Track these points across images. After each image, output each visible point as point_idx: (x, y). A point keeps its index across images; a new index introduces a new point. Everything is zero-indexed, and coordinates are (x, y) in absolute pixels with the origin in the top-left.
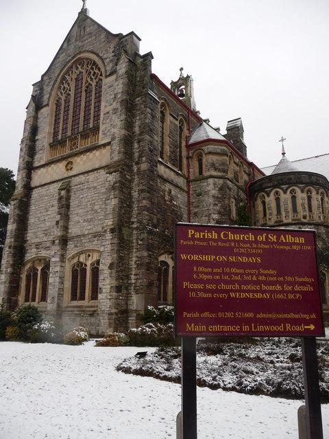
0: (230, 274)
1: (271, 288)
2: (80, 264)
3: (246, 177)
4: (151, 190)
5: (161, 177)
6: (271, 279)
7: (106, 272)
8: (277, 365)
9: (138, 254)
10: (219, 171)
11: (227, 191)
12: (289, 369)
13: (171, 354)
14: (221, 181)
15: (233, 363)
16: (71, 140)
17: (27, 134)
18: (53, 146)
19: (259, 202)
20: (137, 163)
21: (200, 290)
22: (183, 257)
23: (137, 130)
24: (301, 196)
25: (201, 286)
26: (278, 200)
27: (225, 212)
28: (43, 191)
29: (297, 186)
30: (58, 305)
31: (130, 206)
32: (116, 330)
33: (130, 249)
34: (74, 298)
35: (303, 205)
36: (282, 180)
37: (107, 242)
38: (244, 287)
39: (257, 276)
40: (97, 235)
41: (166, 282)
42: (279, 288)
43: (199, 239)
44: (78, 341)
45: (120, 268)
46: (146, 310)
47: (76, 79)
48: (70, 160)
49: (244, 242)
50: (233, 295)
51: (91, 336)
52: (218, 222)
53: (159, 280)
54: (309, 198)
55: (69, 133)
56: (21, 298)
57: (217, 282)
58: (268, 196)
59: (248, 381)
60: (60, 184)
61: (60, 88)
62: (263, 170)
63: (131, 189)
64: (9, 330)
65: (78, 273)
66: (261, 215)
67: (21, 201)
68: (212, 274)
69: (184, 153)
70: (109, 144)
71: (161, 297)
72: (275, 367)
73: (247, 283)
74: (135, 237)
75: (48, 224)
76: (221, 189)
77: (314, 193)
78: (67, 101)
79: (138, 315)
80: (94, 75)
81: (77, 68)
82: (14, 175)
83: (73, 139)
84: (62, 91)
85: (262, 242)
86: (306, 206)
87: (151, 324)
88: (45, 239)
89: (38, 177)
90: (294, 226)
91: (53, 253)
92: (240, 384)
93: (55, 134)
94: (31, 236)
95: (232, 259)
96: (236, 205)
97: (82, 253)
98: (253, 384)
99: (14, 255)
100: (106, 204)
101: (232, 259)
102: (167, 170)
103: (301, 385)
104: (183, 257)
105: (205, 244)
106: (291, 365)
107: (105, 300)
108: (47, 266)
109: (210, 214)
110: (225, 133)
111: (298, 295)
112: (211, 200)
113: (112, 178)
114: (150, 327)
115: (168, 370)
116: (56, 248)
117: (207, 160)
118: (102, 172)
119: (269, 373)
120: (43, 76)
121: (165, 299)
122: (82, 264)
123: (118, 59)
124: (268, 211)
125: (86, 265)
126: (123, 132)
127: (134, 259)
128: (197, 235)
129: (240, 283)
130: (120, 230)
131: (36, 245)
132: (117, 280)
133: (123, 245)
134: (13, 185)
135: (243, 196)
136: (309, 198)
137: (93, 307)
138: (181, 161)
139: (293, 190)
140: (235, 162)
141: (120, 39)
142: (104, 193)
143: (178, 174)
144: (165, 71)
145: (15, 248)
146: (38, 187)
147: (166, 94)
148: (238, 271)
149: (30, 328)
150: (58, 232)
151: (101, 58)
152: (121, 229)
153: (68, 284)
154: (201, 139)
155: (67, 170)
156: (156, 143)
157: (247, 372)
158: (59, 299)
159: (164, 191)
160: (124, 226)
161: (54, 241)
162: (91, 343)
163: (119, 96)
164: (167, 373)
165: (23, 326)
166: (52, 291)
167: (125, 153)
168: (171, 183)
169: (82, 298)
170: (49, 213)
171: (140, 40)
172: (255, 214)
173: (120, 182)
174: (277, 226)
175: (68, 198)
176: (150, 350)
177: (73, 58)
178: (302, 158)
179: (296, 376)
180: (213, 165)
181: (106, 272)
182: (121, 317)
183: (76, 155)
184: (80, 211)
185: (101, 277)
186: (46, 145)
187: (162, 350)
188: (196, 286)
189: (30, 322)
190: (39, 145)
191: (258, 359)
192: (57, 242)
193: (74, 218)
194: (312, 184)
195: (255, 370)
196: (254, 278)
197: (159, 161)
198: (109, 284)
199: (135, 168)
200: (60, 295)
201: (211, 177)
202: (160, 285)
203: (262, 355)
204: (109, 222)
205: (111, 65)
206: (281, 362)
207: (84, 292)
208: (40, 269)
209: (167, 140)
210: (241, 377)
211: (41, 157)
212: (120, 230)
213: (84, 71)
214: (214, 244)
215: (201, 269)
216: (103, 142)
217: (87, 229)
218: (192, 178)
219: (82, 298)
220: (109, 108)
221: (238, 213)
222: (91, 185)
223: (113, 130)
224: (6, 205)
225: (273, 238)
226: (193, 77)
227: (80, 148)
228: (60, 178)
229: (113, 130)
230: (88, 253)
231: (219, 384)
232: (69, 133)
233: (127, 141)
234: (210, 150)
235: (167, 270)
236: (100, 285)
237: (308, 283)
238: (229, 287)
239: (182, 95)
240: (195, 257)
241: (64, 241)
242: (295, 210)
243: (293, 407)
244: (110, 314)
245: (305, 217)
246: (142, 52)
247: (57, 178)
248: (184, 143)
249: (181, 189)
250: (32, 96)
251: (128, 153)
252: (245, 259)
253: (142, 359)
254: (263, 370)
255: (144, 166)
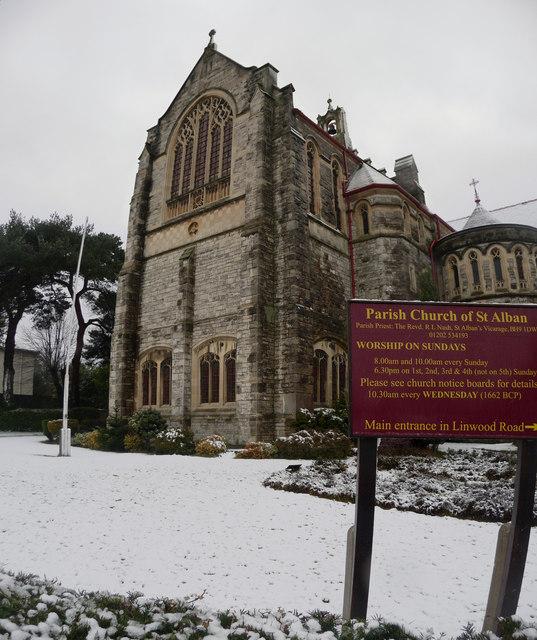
0: (423, 367)
1: (480, 385)
2: (210, 355)
3: (428, 235)
4: (301, 256)
5: (313, 238)
6: (480, 372)
7: (244, 365)
8: (470, 483)
9: (286, 342)
10: (392, 227)
11: (404, 253)
12: (485, 487)
13: (332, 467)
14: (395, 241)
15: (412, 480)
16: (194, 195)
17: (138, 190)
18: (170, 204)
19: (448, 266)
20: (281, 222)
21: (383, 389)
22: (360, 345)
23: (278, 178)
24: (507, 258)
25: (384, 384)
26: (474, 264)
27: (402, 282)
28: (160, 261)
29: (477, 248)
30: (186, 408)
31: (274, 279)
32: (260, 439)
33: (275, 335)
34: (204, 399)
35: (510, 269)
36: (479, 236)
37: (245, 327)
38: (442, 384)
39: (461, 369)
40: (231, 318)
41: (324, 378)
42: (489, 384)
43: (381, 321)
44: (214, 453)
45: (263, 359)
46: (298, 412)
47: (201, 121)
48: (193, 220)
49: (442, 323)
50: (426, 394)
51: (230, 446)
52: (392, 297)
53: (315, 374)
54: (519, 260)
55: (191, 187)
56: (138, 400)
57: (406, 378)
58: (461, 259)
59: (431, 501)
60: (182, 251)
61: (180, 132)
62: (450, 224)
63: (275, 255)
64: (128, 439)
65: (209, 367)
66: (451, 285)
67: (132, 276)
68: (399, 366)
69: (342, 205)
70: (243, 197)
71: (318, 397)
72: (465, 485)
73: (446, 378)
74: (281, 319)
75: (167, 305)
76: (395, 252)
77: (525, 253)
78: (189, 147)
79: (288, 420)
80: (222, 115)
81: (202, 109)
82: (121, 243)
83: (196, 193)
84: (184, 137)
85: (468, 323)
86: (516, 271)
87: (305, 431)
88: (164, 324)
89: (154, 245)
90: (498, 300)
91: (175, 343)
92: (420, 503)
93: (174, 188)
94: (145, 321)
95: (427, 347)
96: (417, 273)
97: (212, 341)
98: (437, 504)
99: (126, 347)
100: (242, 277)
101: (427, 347)
102: (322, 229)
103: (499, 505)
104: (360, 345)
105: (389, 327)
106: (487, 483)
107: (245, 402)
108: (168, 360)
109: (382, 286)
110: (394, 175)
111: (516, 394)
112: (382, 267)
113: (250, 242)
114: (304, 435)
115: (328, 486)
116: (179, 337)
117: (374, 213)
118: (236, 234)
119: (459, 492)
120: (160, 120)
121: (323, 400)
122: (213, 355)
123: (252, 95)
124: (461, 280)
125: (218, 357)
126: (262, 181)
127: (281, 348)
128: (379, 316)
129: (437, 378)
130: (262, 310)
131: (153, 333)
132: (260, 375)
133: (266, 331)
134: (121, 255)
135: (425, 259)
136: (519, 260)
137: (230, 410)
138: (339, 216)
139: (496, 250)
140: (411, 215)
141: (254, 72)
142: (240, 262)
143: (335, 233)
144: (310, 104)
145: (127, 336)
146: (154, 257)
147: (313, 133)
148: (435, 363)
149: (154, 436)
150: (180, 315)
151: (231, 95)
152: (262, 309)
153: (196, 382)
154: (361, 186)
155: (190, 233)
156: (303, 193)
157: (430, 490)
158: (185, 401)
159: (318, 257)
160: (267, 305)
161: (175, 328)
162: (230, 454)
163: (254, 137)
164: (327, 490)
165: (145, 434)
166: (177, 391)
167: (265, 208)
168: (327, 245)
169: (216, 399)
170: (168, 290)
171: (277, 71)
172: (444, 284)
173: (260, 246)
174: (475, 299)
175: (192, 270)
176: (305, 464)
177: (197, 97)
178: (505, 207)
179: (494, 496)
180: (382, 220)
181: (244, 365)
182: (267, 422)
183: (201, 213)
184: (208, 287)
185: (239, 373)
186: (164, 205)
187: (320, 463)
188: (377, 384)
189: (153, 429)
190: (153, 203)
191: (445, 475)
192: (180, 327)
193: (200, 296)
194: (521, 240)
195: (440, 488)
196: (457, 372)
197: (309, 216)
198: (250, 381)
199: (279, 228)
200: (187, 396)
201: (381, 235)
202: (315, 382)
203: (450, 471)
204: (247, 300)
205: (243, 102)
206: (475, 479)
207: (218, 377)
208: (159, 363)
209: (318, 189)
210: (422, 495)
211: (156, 219)
212: (262, 310)
213: (210, 111)
214: (403, 327)
215: (384, 361)
216: (236, 196)
217: (218, 309)
218: (354, 238)
219: (216, 399)
220: (242, 153)
221: (422, 284)
222: (222, 253)
223: (247, 180)
224: (113, 281)
225: (484, 318)
226: (346, 109)
227: (206, 204)
228: (182, 244)
229: (247, 180)
230: (220, 341)
231: (393, 504)
232: (191, 187)
233: (267, 193)
234: (377, 200)
235: (324, 362)
236: (238, 382)
237: (531, 377)
238: (421, 384)
239: (333, 132)
240: (376, 345)
241: (189, 327)
242: (499, 277)
243: (489, 533)
244: (253, 419)
245: (514, 286)
246: (281, 84)
247: (177, 245)
248: (340, 192)
249: (340, 253)
250: (147, 143)
251: (268, 207)
252: (444, 347)
253: (294, 474)
254: (451, 488)
255: (291, 225)
